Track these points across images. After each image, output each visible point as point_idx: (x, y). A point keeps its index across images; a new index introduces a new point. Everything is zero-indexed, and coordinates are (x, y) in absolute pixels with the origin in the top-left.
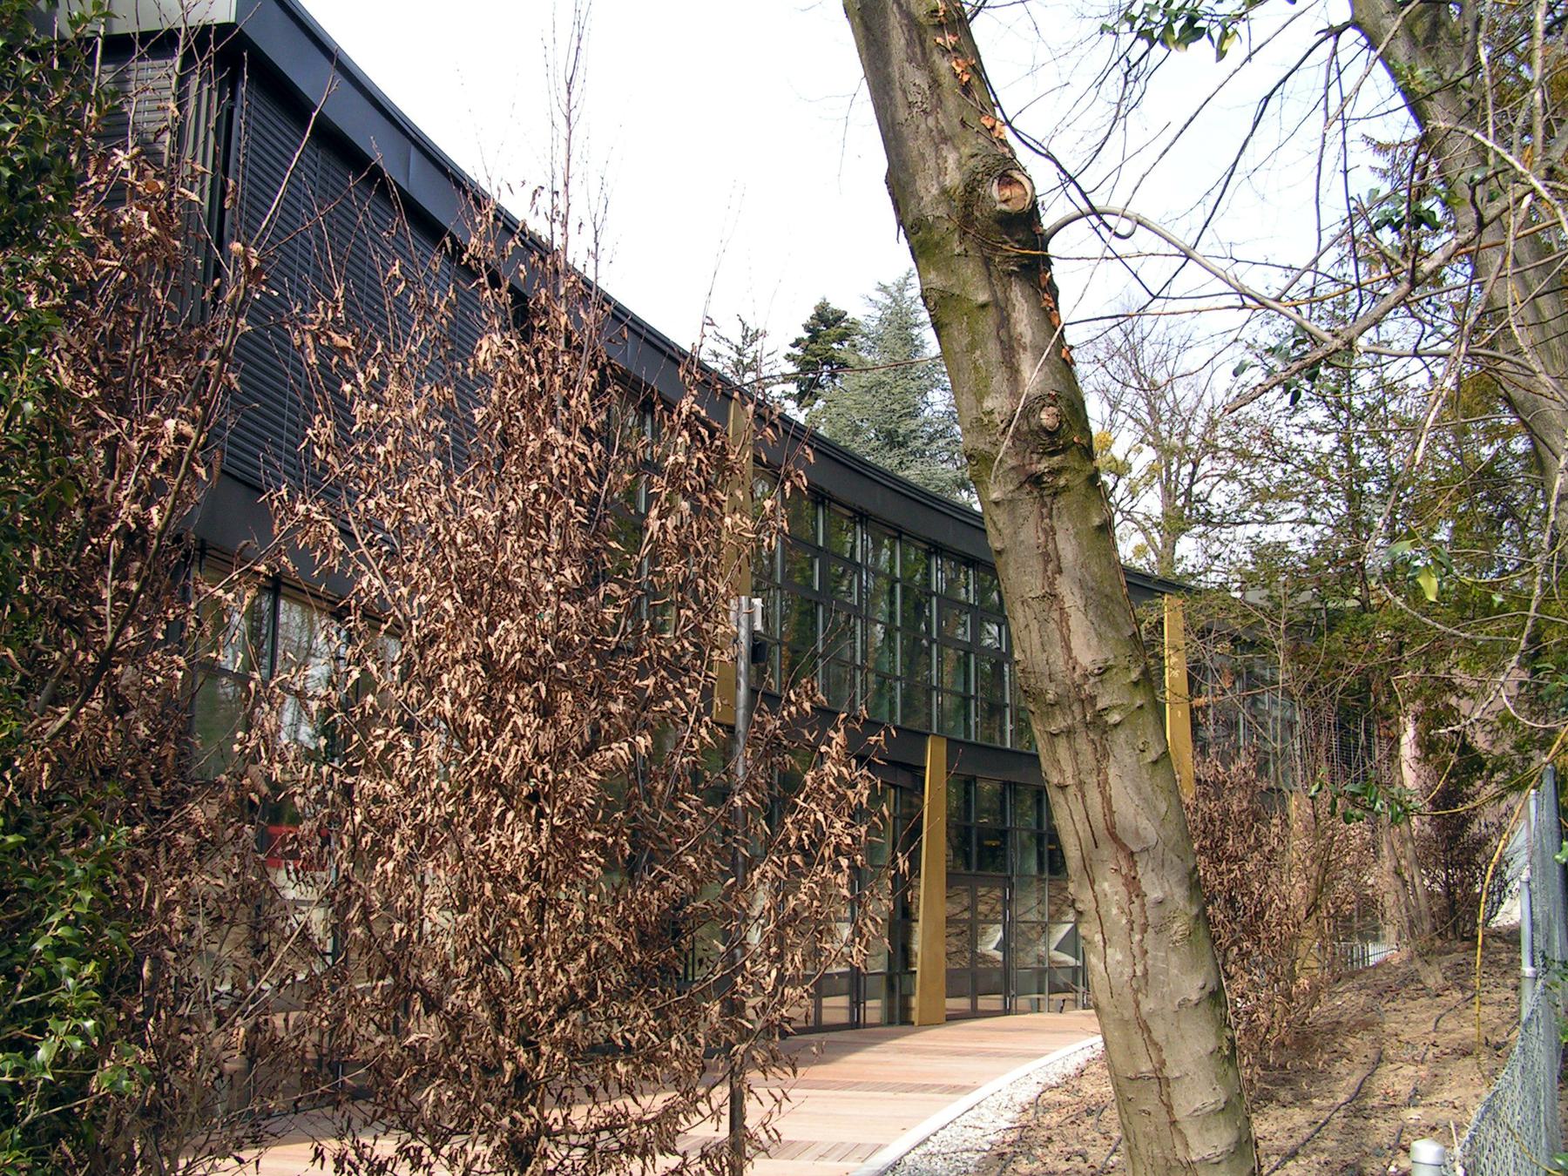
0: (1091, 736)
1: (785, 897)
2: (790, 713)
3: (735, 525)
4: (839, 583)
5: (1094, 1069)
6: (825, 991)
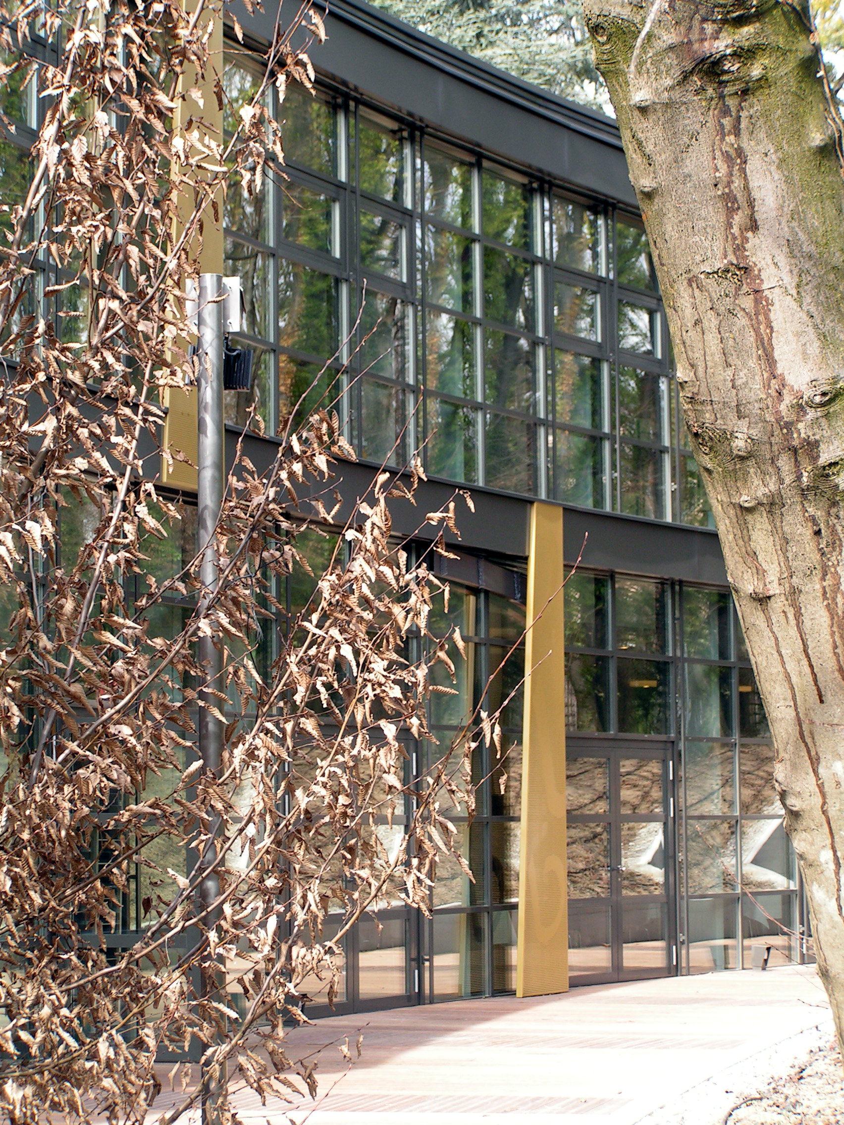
0: (811, 510)
1: (290, 790)
2: (292, 475)
3: (190, 151)
4: (377, 244)
5: (820, 1066)
6: (363, 941)
